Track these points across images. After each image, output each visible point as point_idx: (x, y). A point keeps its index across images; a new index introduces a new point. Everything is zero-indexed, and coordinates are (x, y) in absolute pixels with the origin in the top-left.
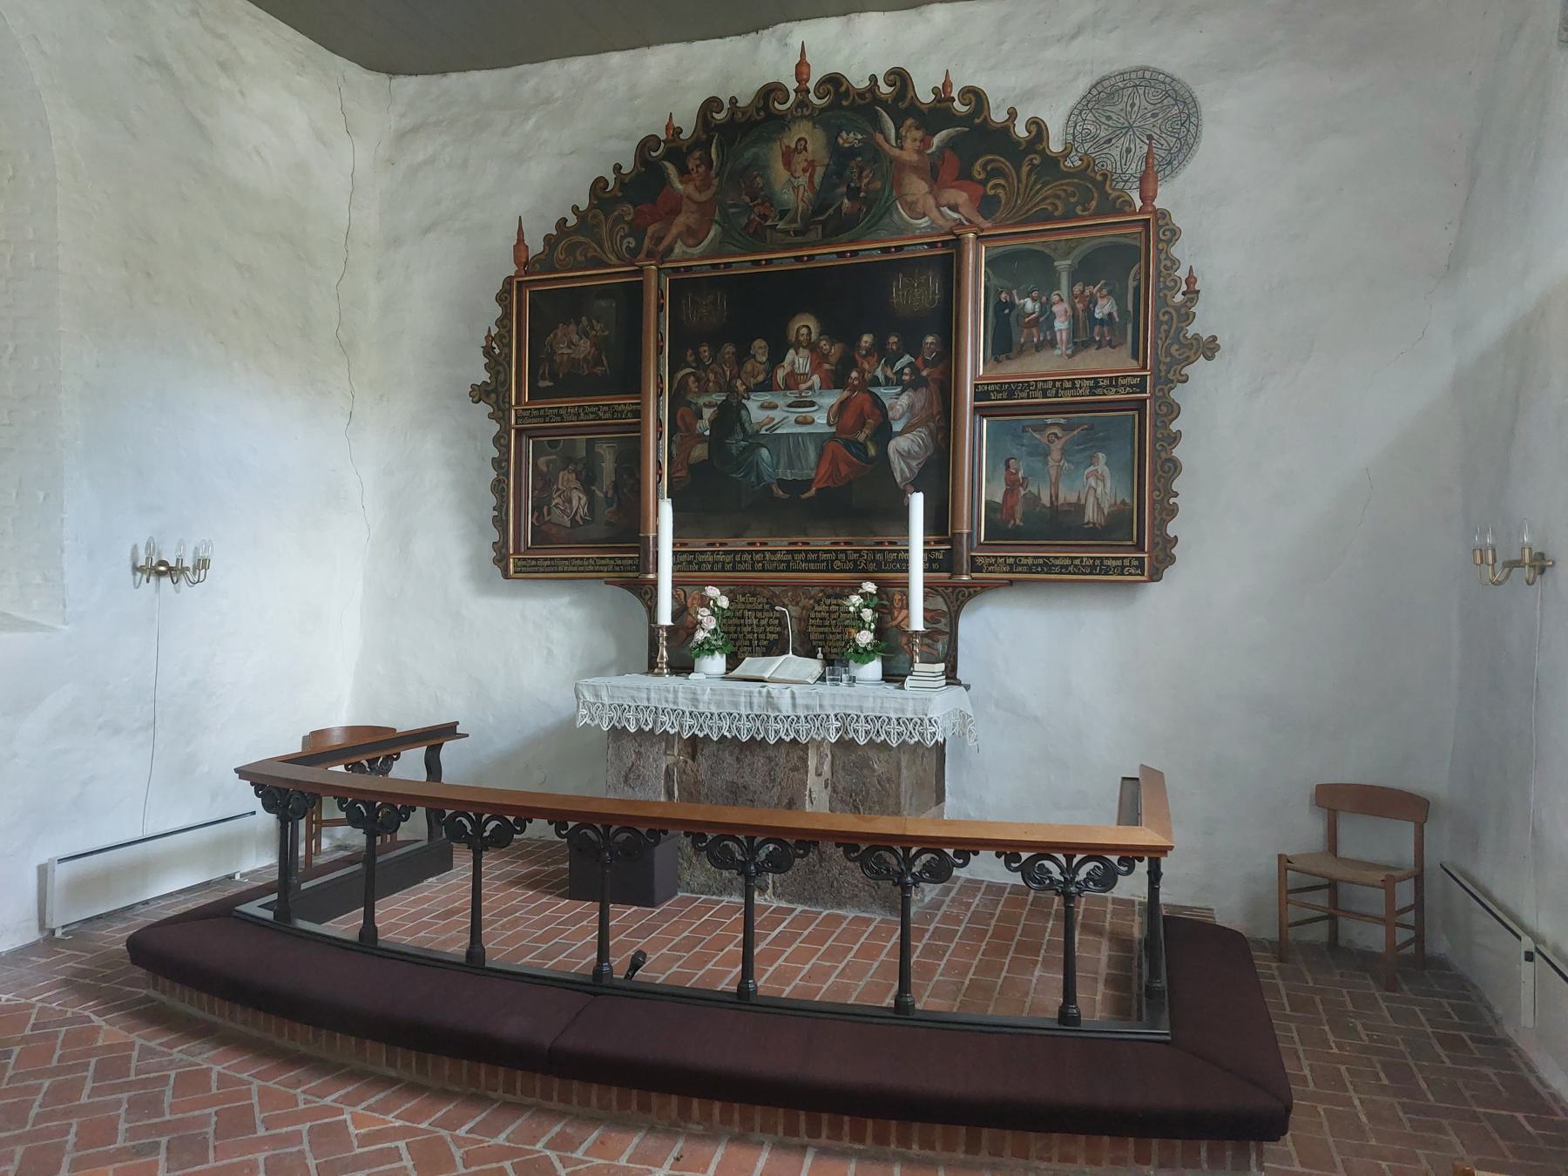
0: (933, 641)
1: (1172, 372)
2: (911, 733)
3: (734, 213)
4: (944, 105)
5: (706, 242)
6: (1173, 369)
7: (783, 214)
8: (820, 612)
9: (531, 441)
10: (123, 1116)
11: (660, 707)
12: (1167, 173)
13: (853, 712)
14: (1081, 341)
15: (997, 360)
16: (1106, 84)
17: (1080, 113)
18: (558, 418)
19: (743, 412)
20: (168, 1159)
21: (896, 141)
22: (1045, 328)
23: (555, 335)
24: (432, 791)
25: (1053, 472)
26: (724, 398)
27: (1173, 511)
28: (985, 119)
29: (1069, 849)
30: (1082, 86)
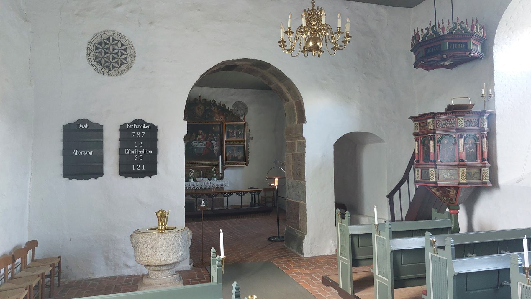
14: (237, 137)
15: (227, 138)
29: (241, 192)
30: (234, 102)
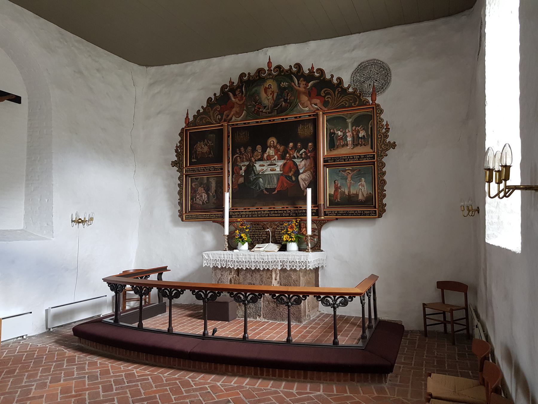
0: (313, 238)
1: (382, 153)
2: (303, 266)
3: (250, 108)
4: (312, 74)
5: (242, 116)
6: (383, 152)
7: (265, 107)
8: (279, 229)
9: (190, 178)
10: (75, 371)
11: (228, 260)
12: (382, 91)
13: (285, 260)
14: (356, 143)
15: (330, 150)
16: (363, 64)
17: (355, 74)
18: (198, 171)
19: (254, 168)
20: (88, 379)
21: (298, 85)
22: (344, 140)
23: (197, 146)
24: (160, 283)
25: (349, 184)
26: (248, 163)
27: (384, 196)
28: (324, 78)
29: (335, 294)
30: (356, 65)
